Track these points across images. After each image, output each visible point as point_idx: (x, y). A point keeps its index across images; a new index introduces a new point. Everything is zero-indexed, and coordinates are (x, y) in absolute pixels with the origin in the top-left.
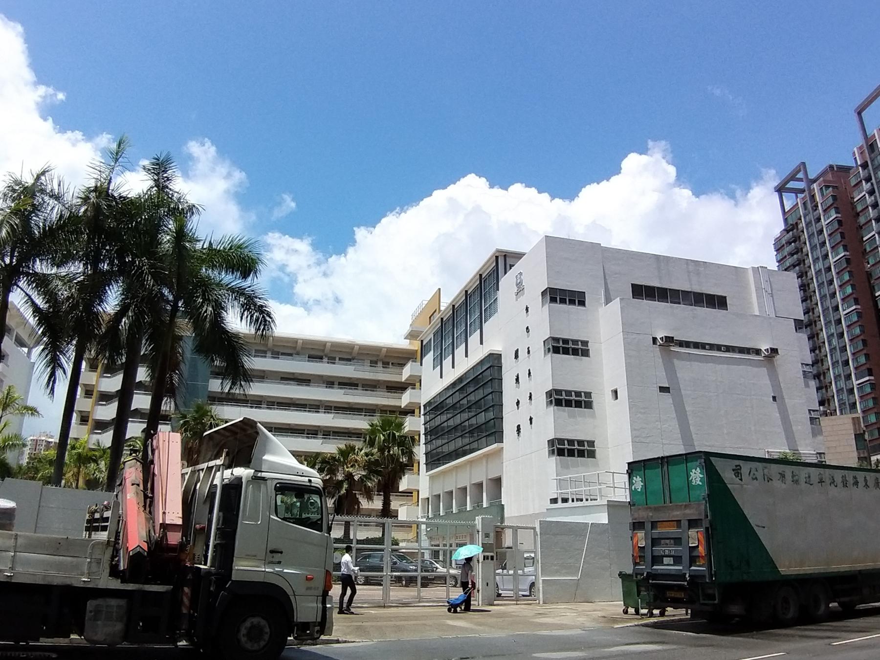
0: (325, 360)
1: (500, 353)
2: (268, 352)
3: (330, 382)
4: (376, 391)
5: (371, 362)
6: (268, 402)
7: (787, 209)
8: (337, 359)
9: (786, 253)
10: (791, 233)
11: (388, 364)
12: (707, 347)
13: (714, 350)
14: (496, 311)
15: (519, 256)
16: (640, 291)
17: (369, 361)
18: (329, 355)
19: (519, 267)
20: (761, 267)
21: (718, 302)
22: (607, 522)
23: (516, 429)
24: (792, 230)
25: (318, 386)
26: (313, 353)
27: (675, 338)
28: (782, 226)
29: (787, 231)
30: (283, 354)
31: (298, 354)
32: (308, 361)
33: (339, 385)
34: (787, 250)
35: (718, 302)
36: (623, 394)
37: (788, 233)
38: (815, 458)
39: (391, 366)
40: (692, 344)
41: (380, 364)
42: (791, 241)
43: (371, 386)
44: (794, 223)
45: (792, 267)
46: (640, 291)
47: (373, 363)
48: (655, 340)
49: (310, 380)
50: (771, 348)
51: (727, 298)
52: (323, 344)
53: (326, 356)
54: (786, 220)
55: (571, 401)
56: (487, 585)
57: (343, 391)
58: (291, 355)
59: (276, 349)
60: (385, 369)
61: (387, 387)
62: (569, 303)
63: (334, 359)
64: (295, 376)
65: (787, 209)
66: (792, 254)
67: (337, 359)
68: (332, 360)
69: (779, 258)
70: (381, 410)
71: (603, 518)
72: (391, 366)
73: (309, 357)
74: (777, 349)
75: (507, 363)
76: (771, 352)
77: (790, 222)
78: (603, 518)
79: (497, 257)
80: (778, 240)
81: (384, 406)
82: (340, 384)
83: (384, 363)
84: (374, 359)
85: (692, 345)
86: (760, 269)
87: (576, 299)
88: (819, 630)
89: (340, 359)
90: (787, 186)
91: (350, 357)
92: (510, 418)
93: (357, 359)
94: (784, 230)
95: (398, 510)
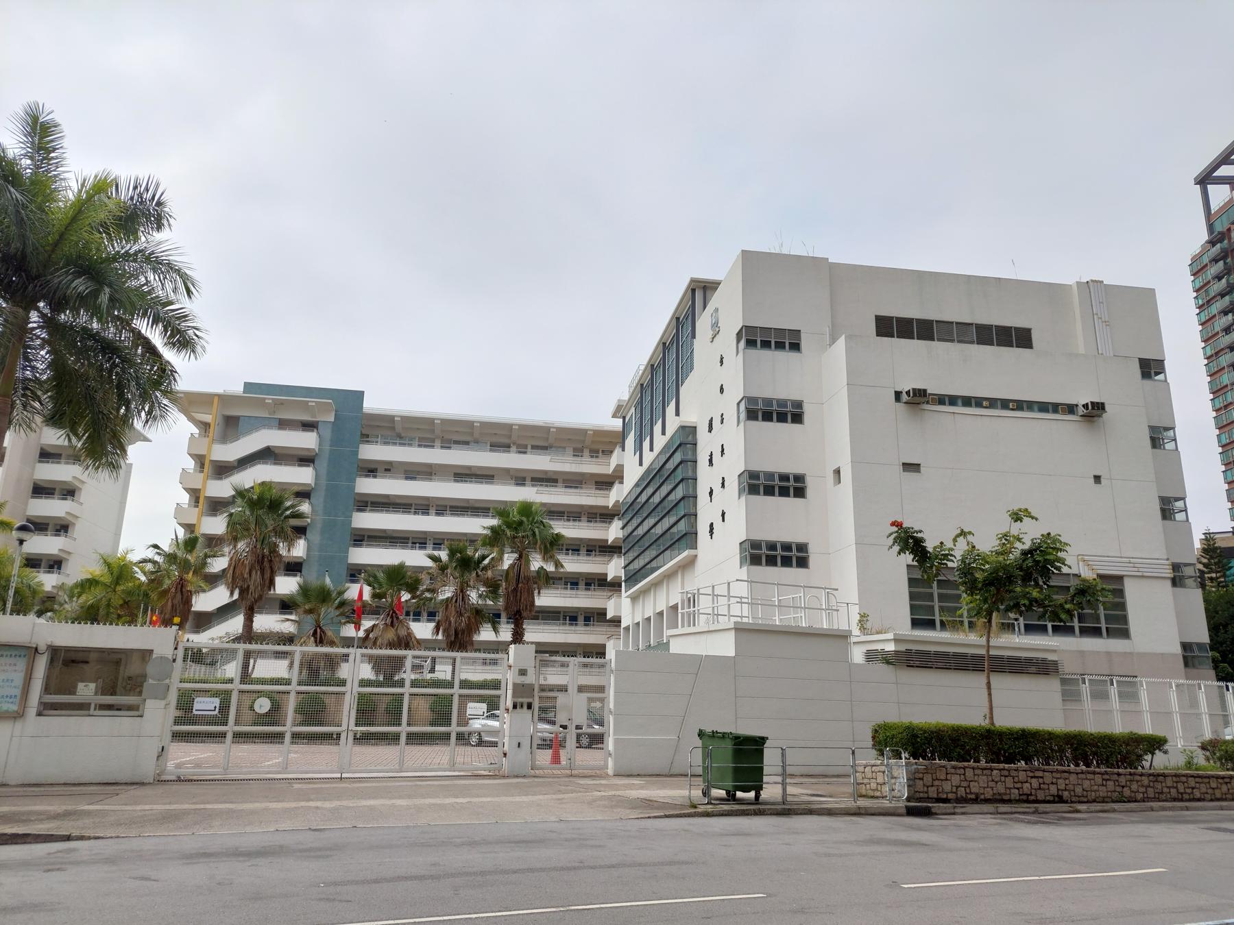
0: (514, 448)
1: (694, 425)
2: (436, 440)
3: (520, 478)
4: (581, 488)
5: (575, 450)
6: (437, 506)
7: (1215, 206)
8: (529, 447)
9: (1210, 277)
10: (1218, 246)
11: (597, 452)
12: (985, 403)
13: (997, 408)
14: (692, 368)
15: (718, 283)
16: (887, 327)
17: (572, 449)
18: (518, 442)
19: (716, 300)
20: (1092, 281)
21: (1020, 338)
22: (732, 654)
23: (714, 531)
24: (1221, 241)
25: (505, 484)
26: (495, 440)
27: (929, 392)
28: (1204, 236)
29: (1212, 243)
30: (457, 442)
31: (477, 442)
32: (491, 450)
33: (531, 481)
34: (1215, 308)
35: (1020, 338)
36: (846, 475)
37: (1213, 246)
38: (1169, 571)
39: (600, 454)
40: (999, 403)
41: (586, 453)
42: (1218, 257)
43: (574, 481)
44: (1225, 230)
45: (1218, 298)
46: (887, 327)
47: (578, 452)
48: (898, 395)
49: (493, 476)
50: (1092, 403)
51: (1032, 332)
52: (507, 428)
53: (514, 444)
54: (1211, 228)
55: (787, 488)
56: (519, 744)
57: (535, 489)
58: (467, 443)
59: (447, 436)
60: (576, 458)
61: (596, 482)
62: (761, 347)
63: (526, 447)
64: (473, 472)
65: (1215, 206)
66: (1219, 278)
67: (529, 447)
68: (522, 450)
69: (1198, 285)
70: (588, 513)
71: (725, 646)
72: (600, 454)
73: (491, 446)
74: (1103, 404)
75: (702, 435)
76: (1093, 408)
77: (1219, 227)
78: (725, 646)
79: (693, 291)
80: (1195, 259)
81: (591, 507)
82: (533, 479)
83: (592, 451)
84: (580, 446)
85: (960, 402)
86: (1091, 284)
87: (789, 341)
88: (1075, 819)
89: (533, 447)
90: (1216, 174)
91: (546, 445)
92: (706, 512)
93: (555, 447)
94: (1207, 242)
95: (605, 645)
